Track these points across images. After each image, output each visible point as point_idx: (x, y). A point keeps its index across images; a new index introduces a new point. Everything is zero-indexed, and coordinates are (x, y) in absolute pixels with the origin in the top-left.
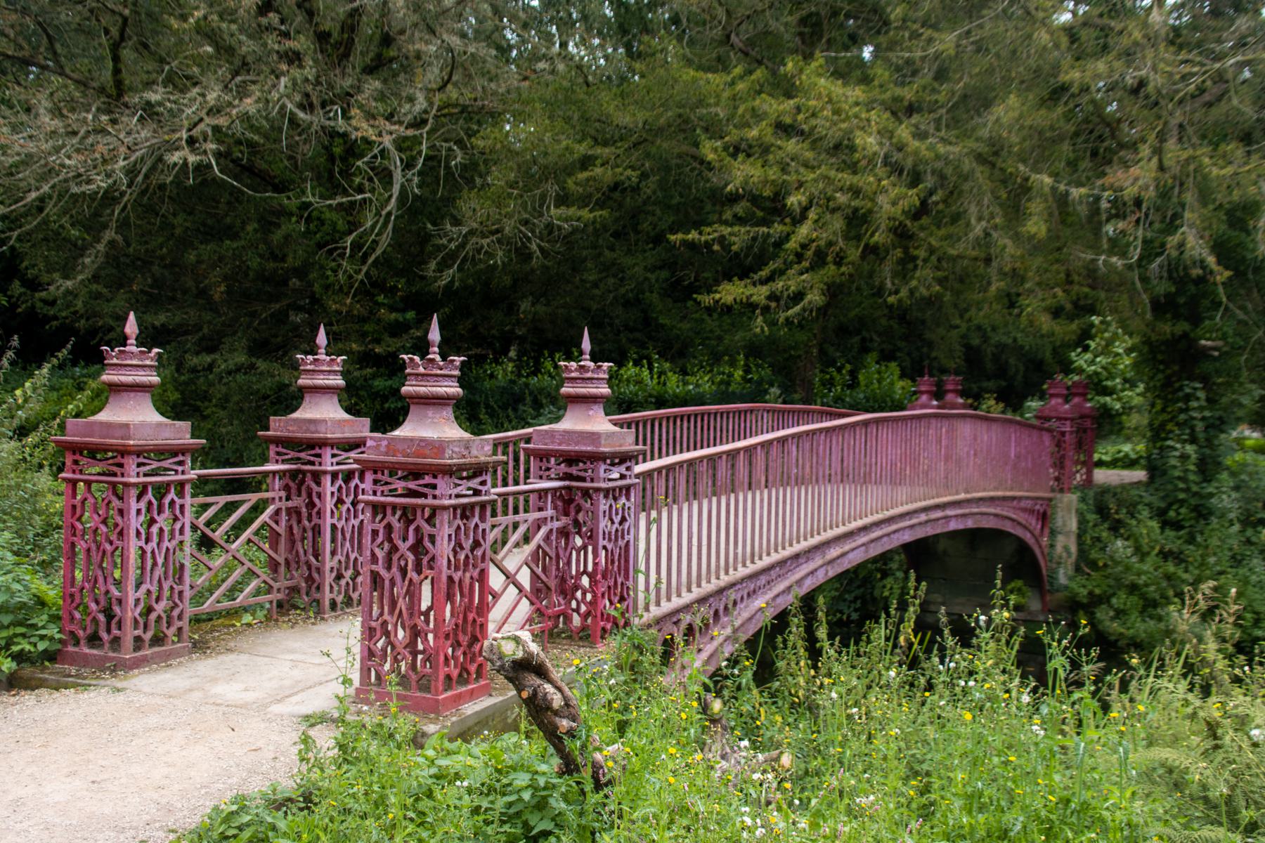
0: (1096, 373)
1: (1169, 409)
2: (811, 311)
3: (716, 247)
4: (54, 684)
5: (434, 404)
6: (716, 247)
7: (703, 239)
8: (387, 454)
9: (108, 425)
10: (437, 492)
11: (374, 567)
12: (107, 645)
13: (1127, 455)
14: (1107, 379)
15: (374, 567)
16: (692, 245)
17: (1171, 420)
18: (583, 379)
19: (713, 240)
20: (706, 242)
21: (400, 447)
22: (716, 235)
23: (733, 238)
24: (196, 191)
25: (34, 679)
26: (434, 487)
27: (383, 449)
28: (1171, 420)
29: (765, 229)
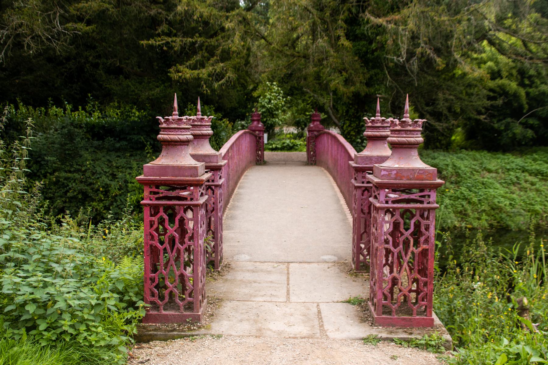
0: (270, 108)
1: (352, 125)
2: (231, 82)
3: (165, 48)
4: (162, 337)
5: (405, 148)
6: (165, 48)
7: (157, 43)
8: (396, 179)
9: (164, 169)
10: (431, 200)
11: (386, 246)
12: (182, 308)
13: (288, 145)
14: (275, 111)
15: (386, 246)
16: (151, 47)
17: (353, 130)
18: (383, 127)
19: (163, 44)
20: (159, 45)
21: (405, 174)
22: (164, 42)
23: (174, 44)
24: (371, 14)
25: (145, 335)
26: (429, 196)
27: (393, 176)
28: (353, 130)
29: (190, 39)
